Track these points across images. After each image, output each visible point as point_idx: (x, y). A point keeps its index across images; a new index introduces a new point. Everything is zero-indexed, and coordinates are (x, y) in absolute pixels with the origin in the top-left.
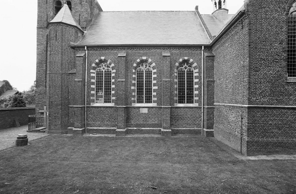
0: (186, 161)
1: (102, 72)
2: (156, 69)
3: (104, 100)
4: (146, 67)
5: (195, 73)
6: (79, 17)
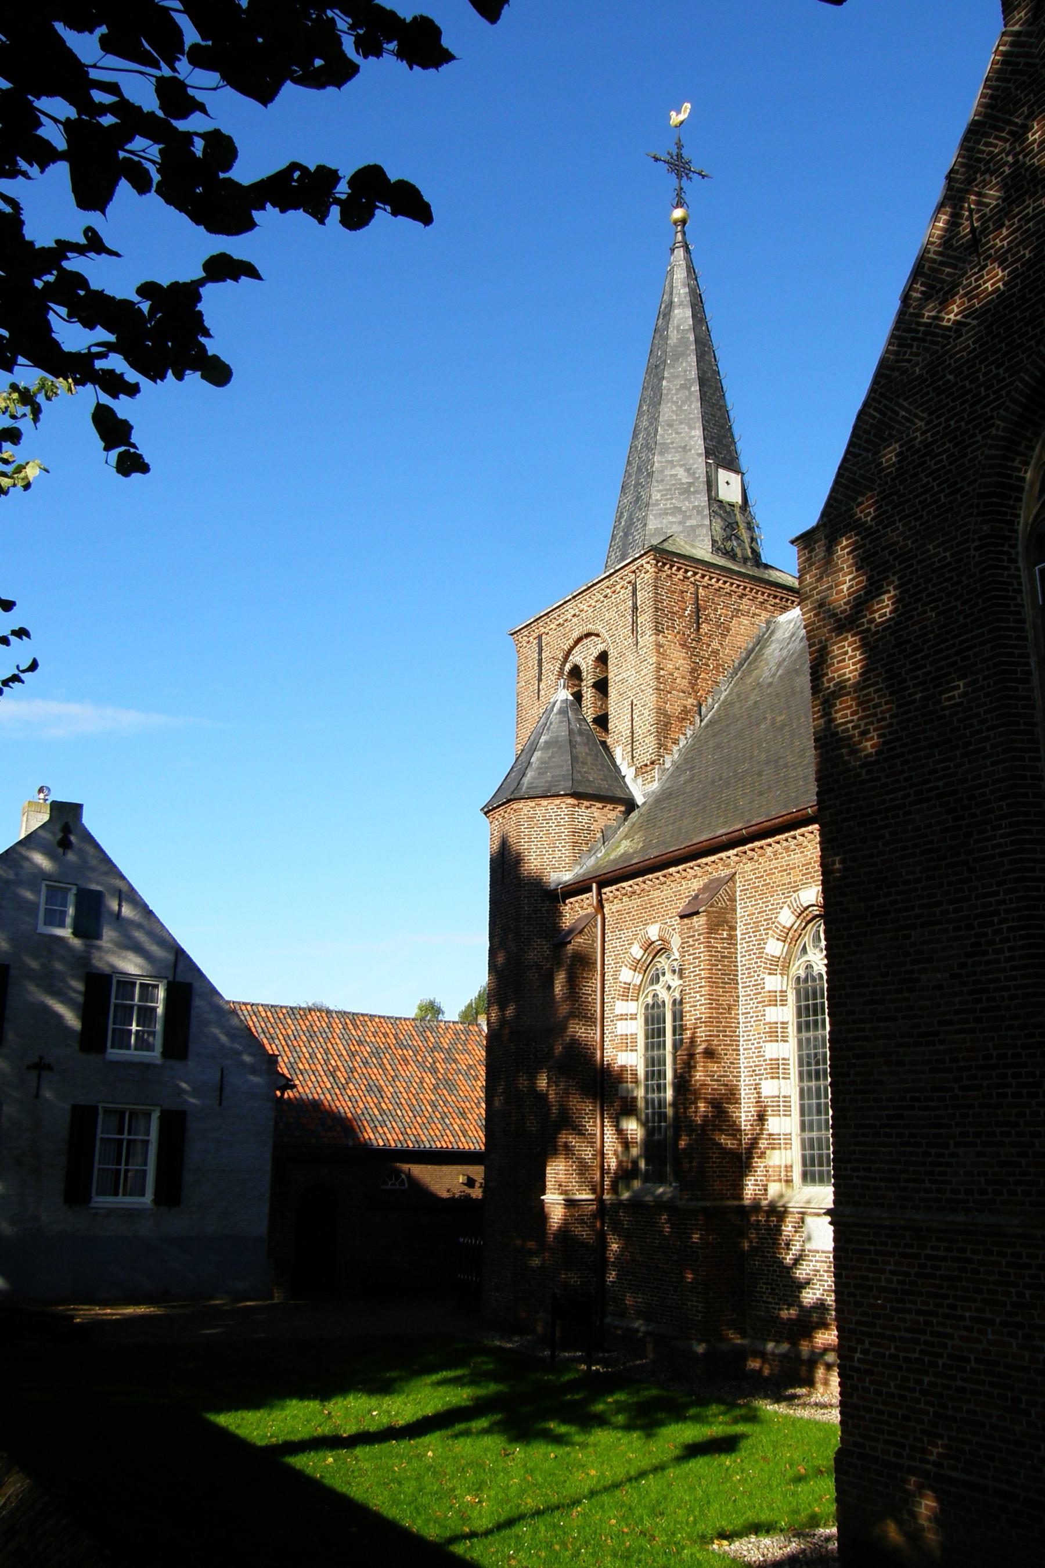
5: (634, 1017)
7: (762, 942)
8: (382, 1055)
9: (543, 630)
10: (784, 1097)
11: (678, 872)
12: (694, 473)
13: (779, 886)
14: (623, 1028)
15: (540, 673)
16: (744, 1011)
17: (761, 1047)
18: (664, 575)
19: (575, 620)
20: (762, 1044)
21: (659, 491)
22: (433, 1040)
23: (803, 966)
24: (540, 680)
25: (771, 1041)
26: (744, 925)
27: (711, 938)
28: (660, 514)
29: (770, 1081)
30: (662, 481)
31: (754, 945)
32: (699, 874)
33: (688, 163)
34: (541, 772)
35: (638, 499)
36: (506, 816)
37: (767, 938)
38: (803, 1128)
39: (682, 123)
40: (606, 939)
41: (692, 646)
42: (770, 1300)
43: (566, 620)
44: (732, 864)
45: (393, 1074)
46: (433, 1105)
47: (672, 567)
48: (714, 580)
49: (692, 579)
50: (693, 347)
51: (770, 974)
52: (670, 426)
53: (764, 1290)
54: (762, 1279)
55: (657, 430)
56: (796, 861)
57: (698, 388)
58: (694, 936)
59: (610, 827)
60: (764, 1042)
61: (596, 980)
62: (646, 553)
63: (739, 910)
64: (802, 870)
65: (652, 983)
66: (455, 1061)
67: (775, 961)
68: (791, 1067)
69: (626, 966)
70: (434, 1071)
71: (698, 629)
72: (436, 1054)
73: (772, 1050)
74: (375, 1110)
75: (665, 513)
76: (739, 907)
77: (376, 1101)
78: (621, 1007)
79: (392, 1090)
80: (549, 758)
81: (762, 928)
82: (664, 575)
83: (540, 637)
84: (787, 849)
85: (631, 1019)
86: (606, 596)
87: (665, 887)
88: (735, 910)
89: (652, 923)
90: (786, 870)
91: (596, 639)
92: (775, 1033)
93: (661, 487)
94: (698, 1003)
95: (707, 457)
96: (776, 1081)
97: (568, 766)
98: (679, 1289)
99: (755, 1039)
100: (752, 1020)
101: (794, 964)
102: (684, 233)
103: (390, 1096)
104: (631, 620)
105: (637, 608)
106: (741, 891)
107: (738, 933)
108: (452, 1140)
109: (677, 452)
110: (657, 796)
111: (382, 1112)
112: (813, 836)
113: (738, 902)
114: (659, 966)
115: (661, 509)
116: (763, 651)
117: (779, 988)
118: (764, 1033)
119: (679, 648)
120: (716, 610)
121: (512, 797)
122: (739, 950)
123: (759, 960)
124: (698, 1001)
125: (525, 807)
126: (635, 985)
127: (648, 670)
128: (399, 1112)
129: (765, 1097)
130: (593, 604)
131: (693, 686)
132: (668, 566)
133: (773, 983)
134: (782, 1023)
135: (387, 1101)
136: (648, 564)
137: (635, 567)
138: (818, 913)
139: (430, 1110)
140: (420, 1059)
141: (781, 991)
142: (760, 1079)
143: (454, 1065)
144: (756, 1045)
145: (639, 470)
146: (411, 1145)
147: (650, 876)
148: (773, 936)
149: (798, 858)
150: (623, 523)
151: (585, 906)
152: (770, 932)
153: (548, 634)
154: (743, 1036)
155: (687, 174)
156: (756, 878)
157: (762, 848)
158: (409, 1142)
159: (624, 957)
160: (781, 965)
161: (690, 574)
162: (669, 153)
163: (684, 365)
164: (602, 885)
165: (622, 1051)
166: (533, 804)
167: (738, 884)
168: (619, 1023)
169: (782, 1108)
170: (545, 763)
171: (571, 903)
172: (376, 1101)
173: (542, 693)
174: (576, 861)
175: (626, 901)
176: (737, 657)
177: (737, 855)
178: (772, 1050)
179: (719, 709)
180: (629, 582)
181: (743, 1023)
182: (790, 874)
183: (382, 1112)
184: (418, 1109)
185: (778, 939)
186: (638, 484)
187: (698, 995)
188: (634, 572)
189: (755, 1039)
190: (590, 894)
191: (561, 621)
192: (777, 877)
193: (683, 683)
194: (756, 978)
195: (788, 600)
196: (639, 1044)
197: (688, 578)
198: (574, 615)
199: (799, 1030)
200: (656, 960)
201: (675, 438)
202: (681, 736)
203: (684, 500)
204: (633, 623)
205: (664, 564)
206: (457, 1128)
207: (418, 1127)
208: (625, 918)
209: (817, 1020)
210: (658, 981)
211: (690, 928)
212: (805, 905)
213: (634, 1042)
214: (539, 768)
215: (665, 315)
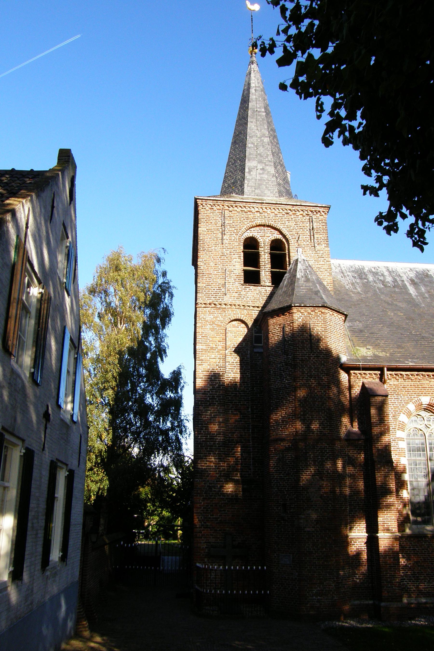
137: (313, 210)
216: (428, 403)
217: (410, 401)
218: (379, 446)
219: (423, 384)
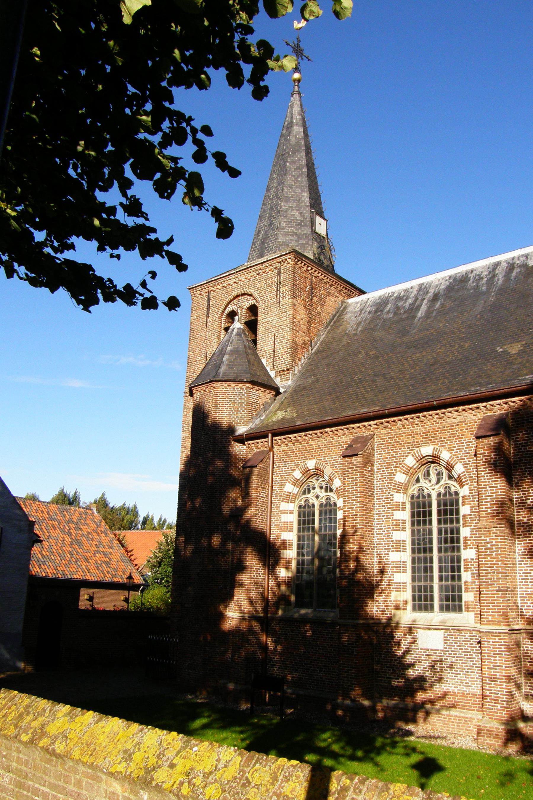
0: (459, 783)
1: (313, 505)
2: (467, 484)
3: (413, 592)
4: (438, 481)
5: (291, 512)
6: (274, 344)
7: (392, 475)
8: (41, 523)
9: (212, 289)
10: (403, 562)
11: (332, 431)
12: (304, 215)
13: (406, 443)
14: (286, 518)
15: (208, 313)
16: (377, 512)
17: (390, 533)
18: (297, 267)
19: (235, 285)
20: (390, 532)
21: (284, 222)
22: (68, 517)
23: (416, 490)
24: (208, 317)
25: (397, 530)
26: (379, 464)
27: (363, 469)
28: (285, 235)
29: (395, 552)
30: (286, 216)
31: (387, 476)
32: (347, 433)
33: (302, 50)
34: (231, 365)
35: (271, 224)
36: (207, 390)
37: (396, 472)
38: (413, 579)
39: (301, 28)
40: (275, 466)
41: (309, 308)
42: (392, 677)
43: (229, 285)
44: (372, 429)
45: (48, 535)
46: (71, 553)
47: (302, 262)
48: (320, 274)
49: (310, 272)
50: (304, 148)
51: (397, 492)
52: (291, 188)
53: (387, 671)
54: (386, 665)
55: (283, 189)
56: (419, 430)
57: (306, 170)
58: (353, 468)
59: (267, 403)
60: (392, 530)
61: (268, 489)
62: (289, 253)
63: (376, 455)
64: (423, 436)
65: (304, 493)
66: (81, 529)
67: (400, 485)
68: (407, 545)
69: (289, 482)
70: (70, 534)
71: (312, 299)
72: (70, 524)
73: (397, 535)
74: (39, 555)
75: (287, 234)
76: (376, 454)
77: (40, 550)
78: (284, 506)
79: (48, 544)
80: (234, 360)
81: (392, 466)
82: (297, 267)
83: (209, 292)
84: (412, 424)
85: (290, 513)
86: (258, 274)
87: (321, 439)
88: (374, 455)
89: (310, 459)
90: (411, 435)
91: (248, 297)
92: (398, 526)
93: (285, 220)
94: (354, 507)
95: (311, 208)
96: (399, 552)
97: (246, 365)
98: (324, 670)
99: (385, 529)
100: (383, 518)
101: (411, 488)
102: (299, 88)
103: (47, 547)
104: (275, 289)
105: (280, 283)
106: (378, 445)
107: (375, 468)
108: (83, 574)
109: (294, 202)
110: (293, 388)
111: (42, 555)
112: (431, 417)
113: (375, 451)
114: (311, 484)
115: (285, 232)
116: (343, 317)
117: (401, 501)
118: (392, 525)
119: (303, 308)
120: (320, 290)
121: (214, 379)
122: (375, 478)
123: (389, 484)
124: (355, 505)
125: (221, 386)
126: (293, 494)
127: (287, 319)
128: (52, 556)
129: (392, 562)
130: (249, 277)
131: (309, 330)
132: (300, 262)
133: (399, 497)
134: (403, 520)
135: (46, 550)
136: (290, 261)
137: (280, 260)
138: (431, 460)
139: (69, 557)
140: (62, 528)
141: (403, 503)
142: (389, 551)
143: (80, 531)
144: (386, 532)
145: (272, 208)
146: (60, 577)
147: (311, 432)
148: (400, 472)
149: (420, 429)
150: (261, 237)
151: (259, 446)
152: (398, 469)
153: (215, 291)
154: (377, 527)
155: (301, 57)
156: (389, 438)
157: (394, 421)
158: (59, 574)
159: (288, 478)
160: (403, 488)
161: (309, 268)
162: (293, 42)
163: (299, 156)
164: (274, 435)
165: (284, 531)
166: (226, 385)
167: (376, 441)
168: (282, 515)
169: (401, 568)
170: (232, 362)
171: (249, 444)
172: (40, 550)
173: (209, 324)
174: (250, 421)
175: (291, 446)
176: (328, 317)
177: (376, 424)
178: (397, 535)
179: (321, 344)
180: (275, 268)
181: (377, 519)
182: (414, 437)
183: (42, 555)
184: (63, 556)
185: (404, 473)
186: (270, 216)
187: (354, 502)
188: (280, 262)
189: (385, 529)
190: (266, 439)
191: (225, 284)
192: (404, 438)
193: (304, 328)
194: (387, 494)
195: (351, 291)
196: (294, 528)
197: (308, 271)
198: (235, 283)
199: (413, 524)
200: (309, 480)
201: (294, 195)
202: (302, 357)
203: (299, 229)
204: (277, 291)
205: (298, 261)
206: (84, 568)
207: (63, 566)
208: (289, 455)
209: (426, 520)
210: (309, 492)
211: (350, 463)
212: (424, 455)
213: (291, 526)
214: (228, 365)
215: (288, 128)
216: (314, 468)
217: (297, 467)
218: (243, 521)
219: (311, 445)
